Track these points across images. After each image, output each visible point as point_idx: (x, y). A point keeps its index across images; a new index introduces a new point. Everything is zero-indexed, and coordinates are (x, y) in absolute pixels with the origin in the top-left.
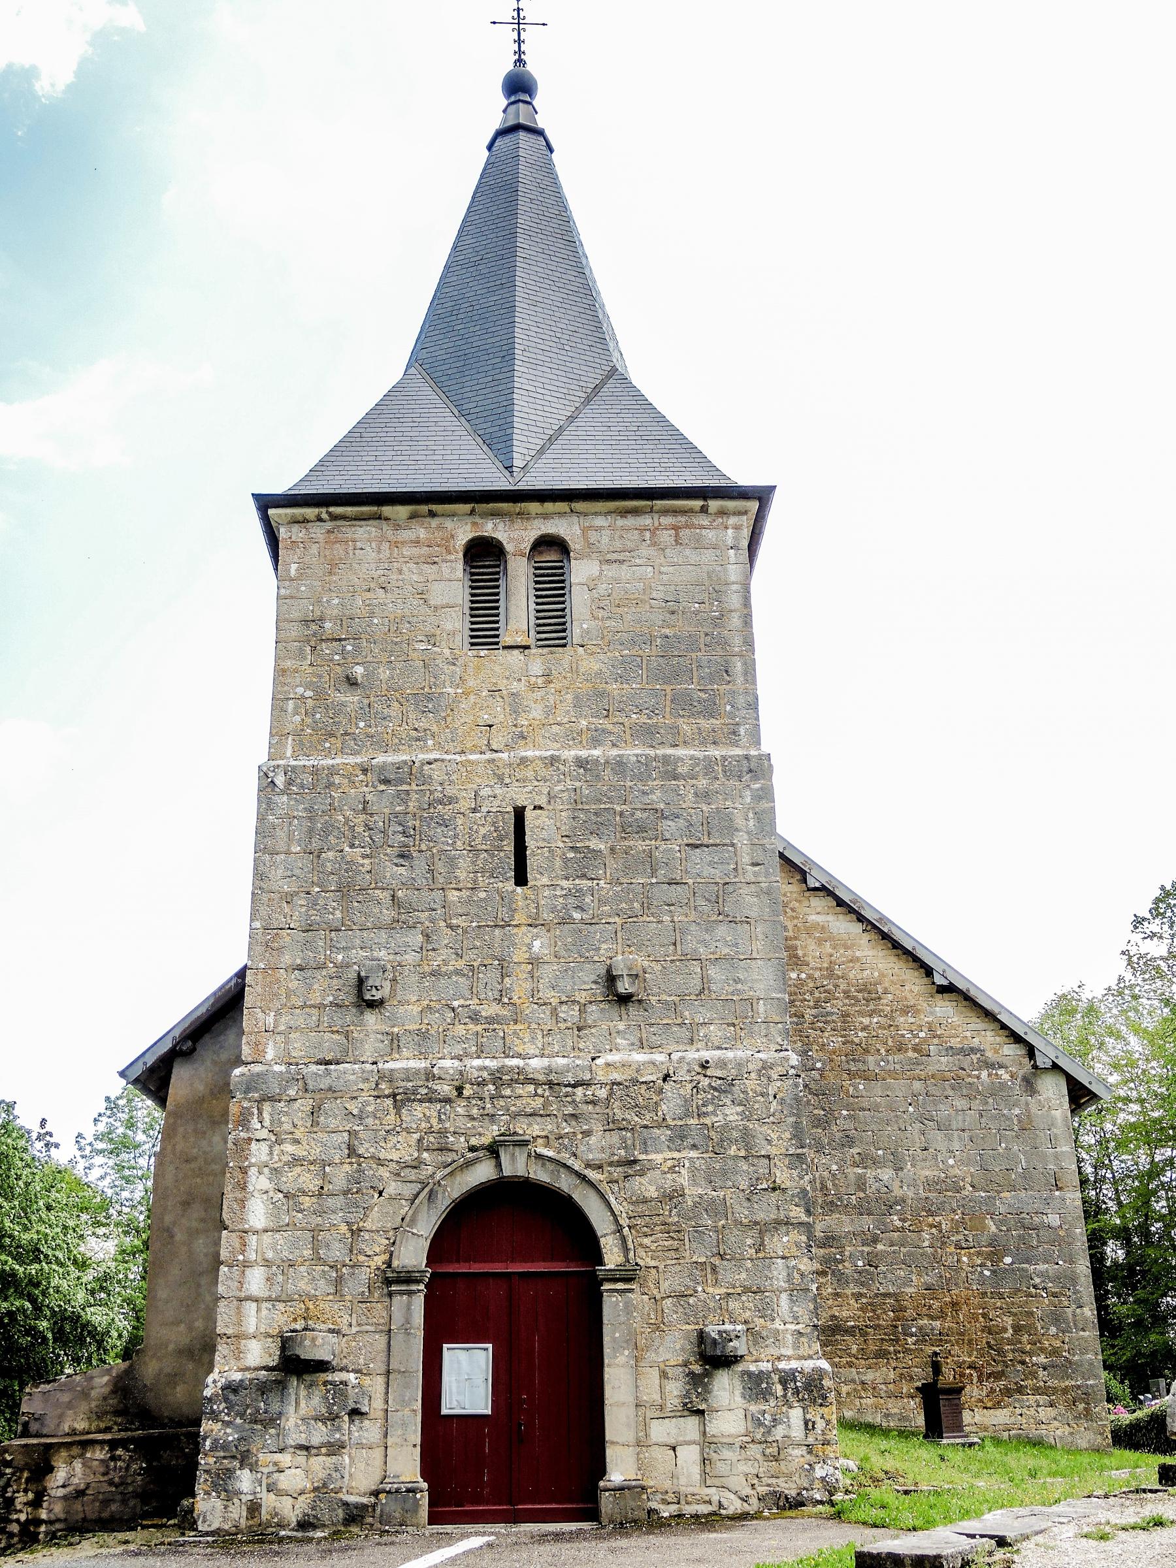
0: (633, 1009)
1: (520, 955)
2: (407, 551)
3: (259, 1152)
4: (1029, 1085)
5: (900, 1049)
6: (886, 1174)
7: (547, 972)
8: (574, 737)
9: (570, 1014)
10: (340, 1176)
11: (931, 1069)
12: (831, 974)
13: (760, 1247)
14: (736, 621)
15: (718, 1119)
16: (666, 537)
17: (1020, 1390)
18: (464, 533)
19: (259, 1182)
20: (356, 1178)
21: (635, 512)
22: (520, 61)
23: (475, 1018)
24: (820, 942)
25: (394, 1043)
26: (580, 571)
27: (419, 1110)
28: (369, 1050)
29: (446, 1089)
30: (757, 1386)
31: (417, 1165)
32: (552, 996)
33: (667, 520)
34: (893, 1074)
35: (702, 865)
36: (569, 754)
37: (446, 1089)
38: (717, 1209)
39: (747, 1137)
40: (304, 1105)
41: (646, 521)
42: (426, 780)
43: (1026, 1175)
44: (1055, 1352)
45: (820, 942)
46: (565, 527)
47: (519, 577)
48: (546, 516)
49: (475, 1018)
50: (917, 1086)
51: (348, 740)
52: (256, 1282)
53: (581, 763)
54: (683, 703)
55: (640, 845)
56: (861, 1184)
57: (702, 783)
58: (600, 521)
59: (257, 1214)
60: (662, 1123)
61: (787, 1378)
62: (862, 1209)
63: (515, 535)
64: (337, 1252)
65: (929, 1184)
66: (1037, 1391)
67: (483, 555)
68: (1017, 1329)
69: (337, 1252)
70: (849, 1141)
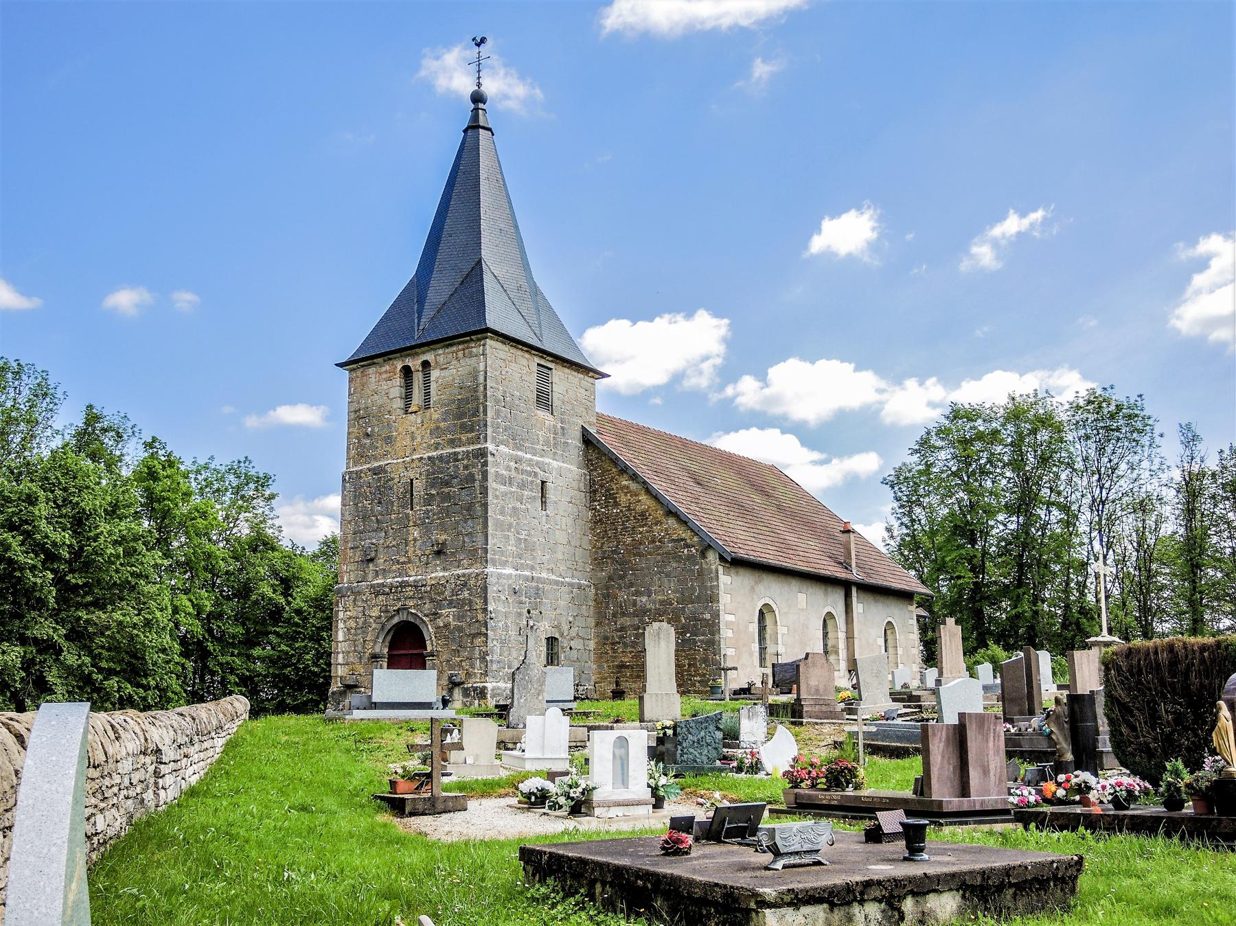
0: (442, 557)
1: (411, 538)
2: (384, 376)
3: (341, 615)
4: (703, 555)
5: (653, 542)
6: (644, 599)
7: (418, 543)
8: (429, 447)
9: (424, 559)
10: (361, 621)
11: (665, 550)
12: (629, 510)
13: (472, 643)
14: (482, 388)
15: (461, 597)
16: (460, 354)
17: (689, 692)
18: (399, 365)
19: (341, 625)
20: (365, 622)
21: (451, 345)
22: (479, 85)
23: (398, 562)
24: (626, 494)
25: (377, 574)
26: (435, 374)
27: (381, 597)
28: (370, 577)
29: (387, 590)
30: (466, 693)
31: (380, 617)
32: (419, 553)
33: (461, 347)
34: (650, 554)
35: (465, 497)
36: (425, 456)
37: (387, 590)
38: (460, 629)
39: (470, 602)
40: (352, 598)
41: (454, 348)
42: (386, 472)
43: (698, 597)
44: (704, 675)
45: (626, 494)
46: (429, 357)
47: (418, 378)
48: (424, 353)
49: (398, 562)
50: (659, 558)
51: (369, 459)
52: (340, 660)
53: (429, 458)
54: (463, 427)
55: (447, 490)
56: (635, 604)
57: (465, 462)
58: (440, 351)
59: (341, 637)
60: (445, 599)
61: (475, 689)
62: (635, 615)
63: (415, 363)
64: (360, 648)
65: (661, 602)
66: (695, 692)
67: (407, 372)
68: (690, 665)
69: (360, 648)
70: (631, 585)
